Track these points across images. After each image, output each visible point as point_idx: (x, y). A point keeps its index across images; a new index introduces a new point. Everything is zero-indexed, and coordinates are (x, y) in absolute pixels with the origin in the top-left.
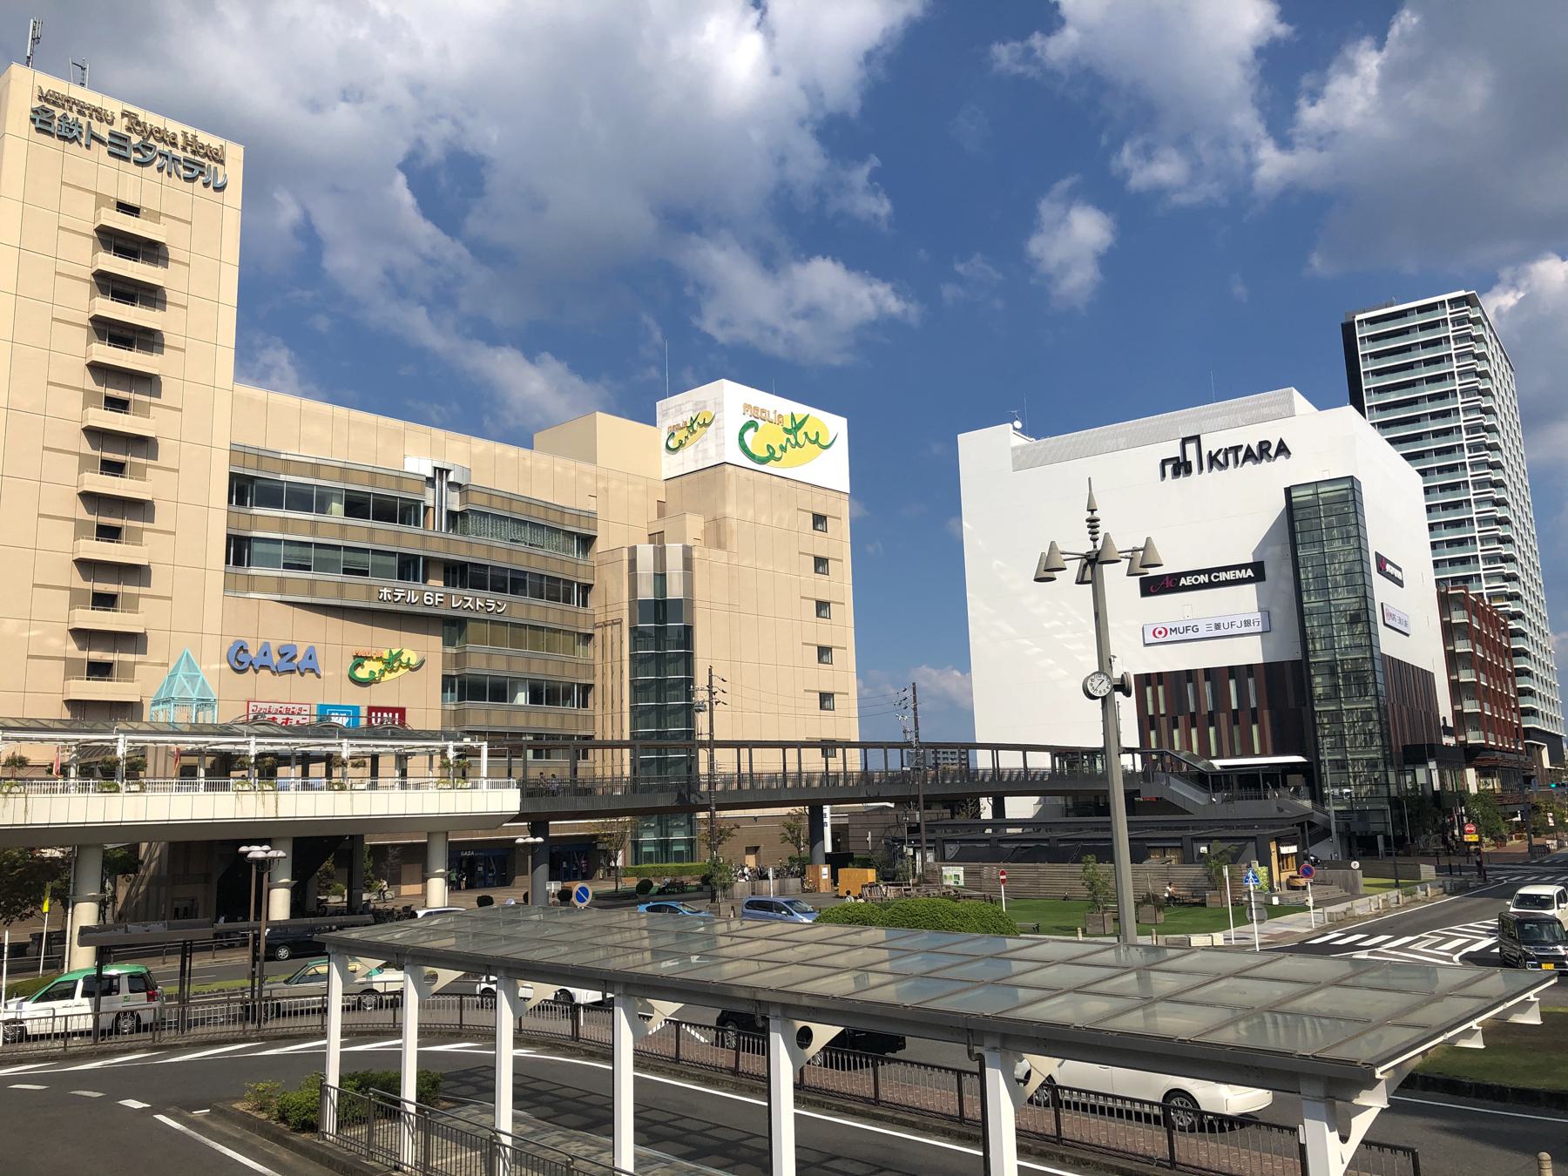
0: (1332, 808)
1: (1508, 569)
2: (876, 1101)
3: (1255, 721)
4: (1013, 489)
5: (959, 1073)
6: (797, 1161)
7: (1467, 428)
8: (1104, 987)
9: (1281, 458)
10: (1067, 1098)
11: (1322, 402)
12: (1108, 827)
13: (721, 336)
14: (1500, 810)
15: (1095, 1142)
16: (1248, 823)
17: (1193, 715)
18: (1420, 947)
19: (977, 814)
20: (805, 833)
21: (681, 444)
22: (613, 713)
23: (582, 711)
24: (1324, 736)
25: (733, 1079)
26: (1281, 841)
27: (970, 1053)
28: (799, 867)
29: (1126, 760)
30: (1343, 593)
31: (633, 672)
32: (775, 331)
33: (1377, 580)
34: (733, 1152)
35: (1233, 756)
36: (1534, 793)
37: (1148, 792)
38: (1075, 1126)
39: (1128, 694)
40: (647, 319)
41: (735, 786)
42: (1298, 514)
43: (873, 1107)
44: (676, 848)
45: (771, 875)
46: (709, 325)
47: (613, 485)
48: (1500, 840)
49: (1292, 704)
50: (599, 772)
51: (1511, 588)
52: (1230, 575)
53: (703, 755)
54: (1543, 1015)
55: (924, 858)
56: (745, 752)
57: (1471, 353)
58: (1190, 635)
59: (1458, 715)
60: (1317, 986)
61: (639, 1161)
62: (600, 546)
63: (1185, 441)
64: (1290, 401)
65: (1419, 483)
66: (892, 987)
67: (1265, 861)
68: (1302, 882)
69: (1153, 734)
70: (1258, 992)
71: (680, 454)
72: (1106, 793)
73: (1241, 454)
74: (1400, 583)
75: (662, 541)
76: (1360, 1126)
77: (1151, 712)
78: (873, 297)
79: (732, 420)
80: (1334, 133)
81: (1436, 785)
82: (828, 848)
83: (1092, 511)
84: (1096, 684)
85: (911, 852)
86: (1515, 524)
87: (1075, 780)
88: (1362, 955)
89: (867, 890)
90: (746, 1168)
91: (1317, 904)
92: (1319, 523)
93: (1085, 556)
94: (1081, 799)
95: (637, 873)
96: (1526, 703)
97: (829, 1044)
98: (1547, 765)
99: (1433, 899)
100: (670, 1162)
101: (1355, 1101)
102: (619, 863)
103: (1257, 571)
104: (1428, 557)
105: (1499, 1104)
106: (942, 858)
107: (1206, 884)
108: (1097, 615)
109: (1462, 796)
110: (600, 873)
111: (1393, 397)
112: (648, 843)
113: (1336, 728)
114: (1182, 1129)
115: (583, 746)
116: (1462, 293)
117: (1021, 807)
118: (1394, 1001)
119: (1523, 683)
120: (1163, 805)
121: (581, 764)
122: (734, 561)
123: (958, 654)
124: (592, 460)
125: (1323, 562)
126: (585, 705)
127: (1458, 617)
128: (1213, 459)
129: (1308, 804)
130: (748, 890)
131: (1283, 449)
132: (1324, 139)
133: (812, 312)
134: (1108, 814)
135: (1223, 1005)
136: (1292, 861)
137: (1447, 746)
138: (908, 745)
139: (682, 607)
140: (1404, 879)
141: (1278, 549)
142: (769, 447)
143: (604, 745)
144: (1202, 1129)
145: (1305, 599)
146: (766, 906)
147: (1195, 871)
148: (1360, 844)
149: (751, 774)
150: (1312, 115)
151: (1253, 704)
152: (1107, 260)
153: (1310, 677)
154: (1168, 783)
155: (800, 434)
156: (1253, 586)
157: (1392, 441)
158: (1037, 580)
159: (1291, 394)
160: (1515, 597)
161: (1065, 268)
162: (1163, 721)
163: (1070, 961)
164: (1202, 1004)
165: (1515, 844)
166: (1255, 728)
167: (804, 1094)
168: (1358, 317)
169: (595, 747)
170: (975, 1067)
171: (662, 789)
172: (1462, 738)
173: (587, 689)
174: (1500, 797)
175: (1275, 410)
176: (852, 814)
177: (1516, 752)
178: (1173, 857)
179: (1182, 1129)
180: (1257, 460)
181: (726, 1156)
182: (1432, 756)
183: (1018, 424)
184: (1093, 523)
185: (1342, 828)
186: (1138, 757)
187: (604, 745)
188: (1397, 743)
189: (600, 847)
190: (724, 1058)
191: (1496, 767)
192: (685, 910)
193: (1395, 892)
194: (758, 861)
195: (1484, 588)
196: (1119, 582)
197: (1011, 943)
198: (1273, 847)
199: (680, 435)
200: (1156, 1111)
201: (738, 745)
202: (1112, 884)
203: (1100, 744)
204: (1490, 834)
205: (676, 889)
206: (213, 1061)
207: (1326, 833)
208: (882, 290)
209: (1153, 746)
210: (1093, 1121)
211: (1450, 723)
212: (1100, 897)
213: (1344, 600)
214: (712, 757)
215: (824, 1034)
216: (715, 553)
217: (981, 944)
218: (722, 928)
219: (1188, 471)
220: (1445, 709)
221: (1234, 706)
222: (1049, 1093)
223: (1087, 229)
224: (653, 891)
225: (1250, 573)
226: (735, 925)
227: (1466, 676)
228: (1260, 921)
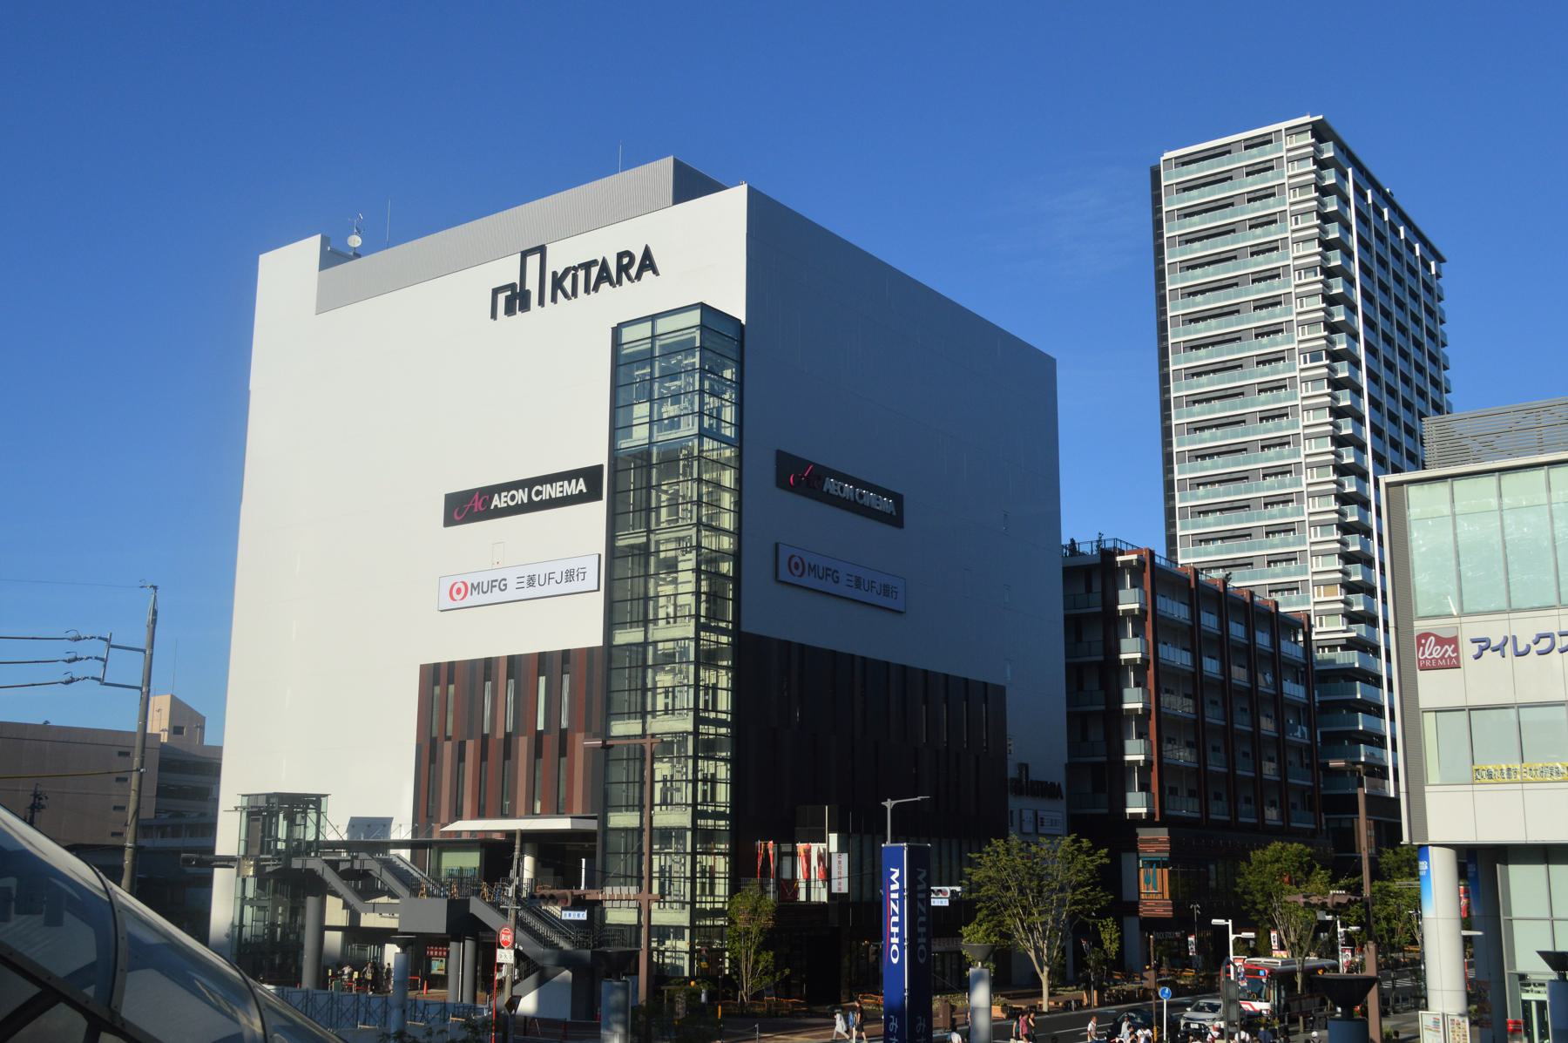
9: (648, 274)
73: (595, 271)
168: (1167, 155)
206: (1455, 463)
219: (525, 307)
221: (540, 727)
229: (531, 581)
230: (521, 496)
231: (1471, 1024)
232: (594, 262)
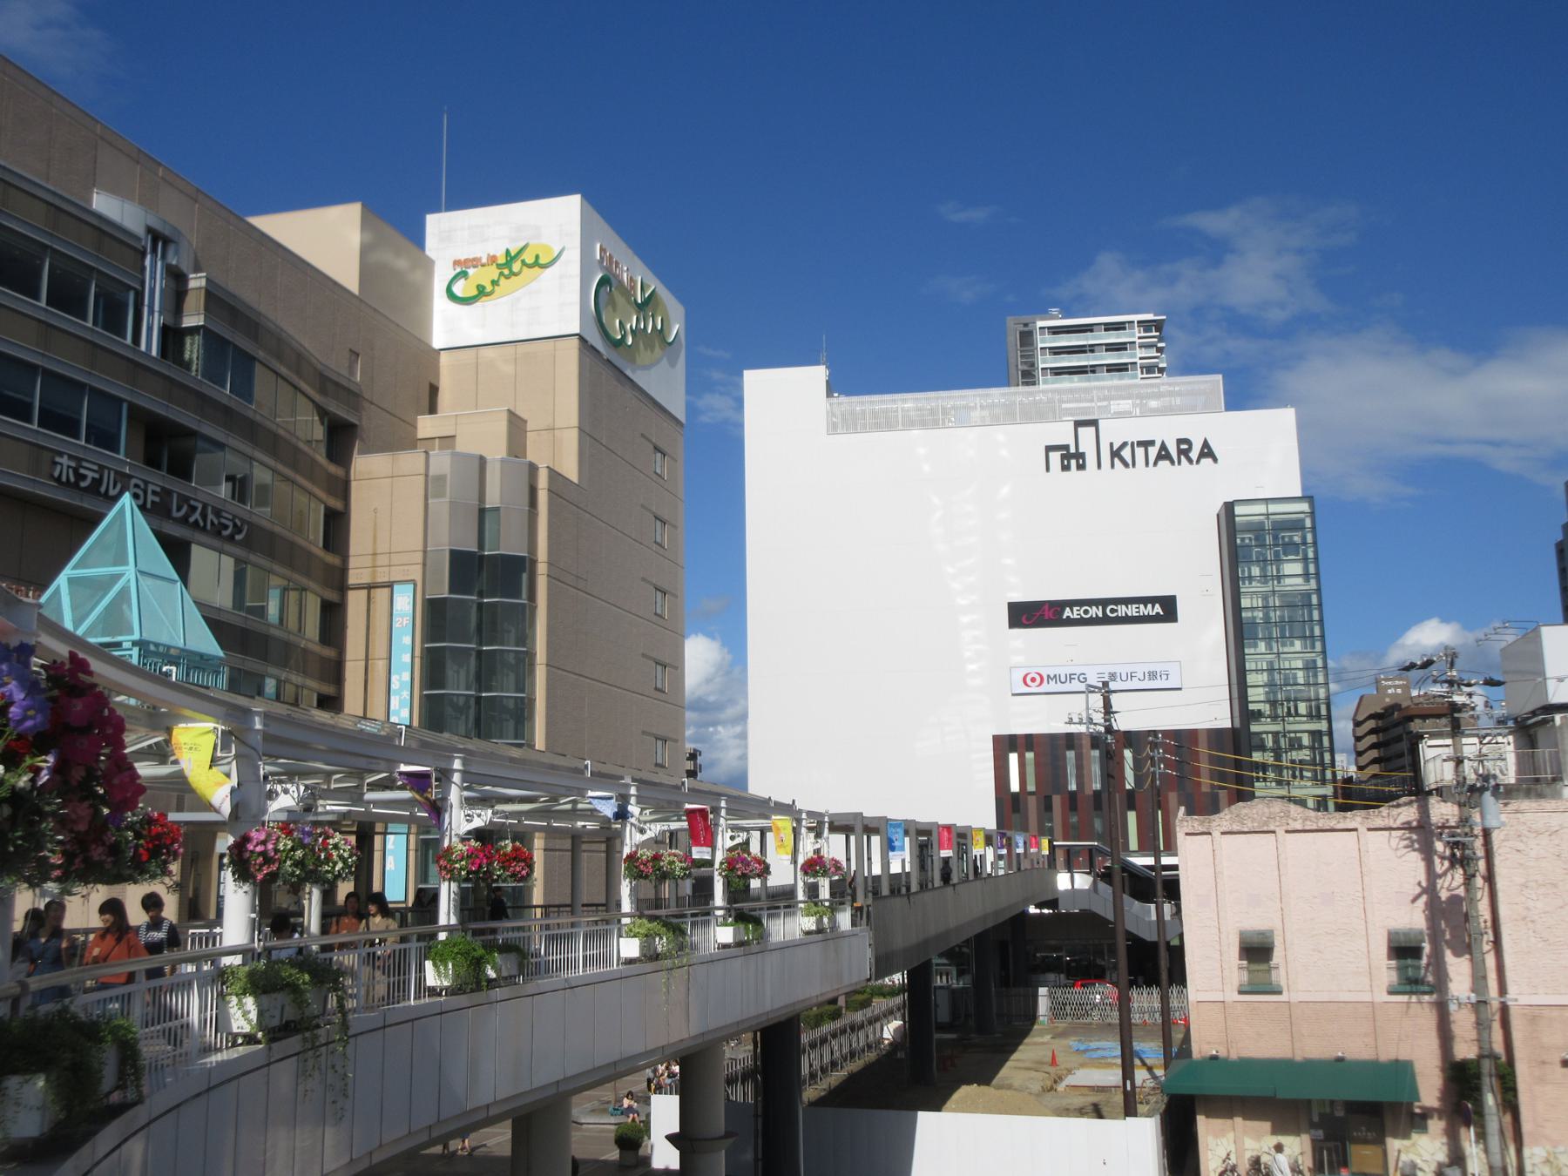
3: (1131, 807)
17: (1073, 795)
21: (482, 292)
52: (1132, 610)
73: (1153, 452)
116: (1150, 317)
128: (1116, 454)
131: (1207, 452)
168: (1040, 324)
199: (484, 276)
225: (1158, 609)
230: (1095, 611)
232: (1152, 443)
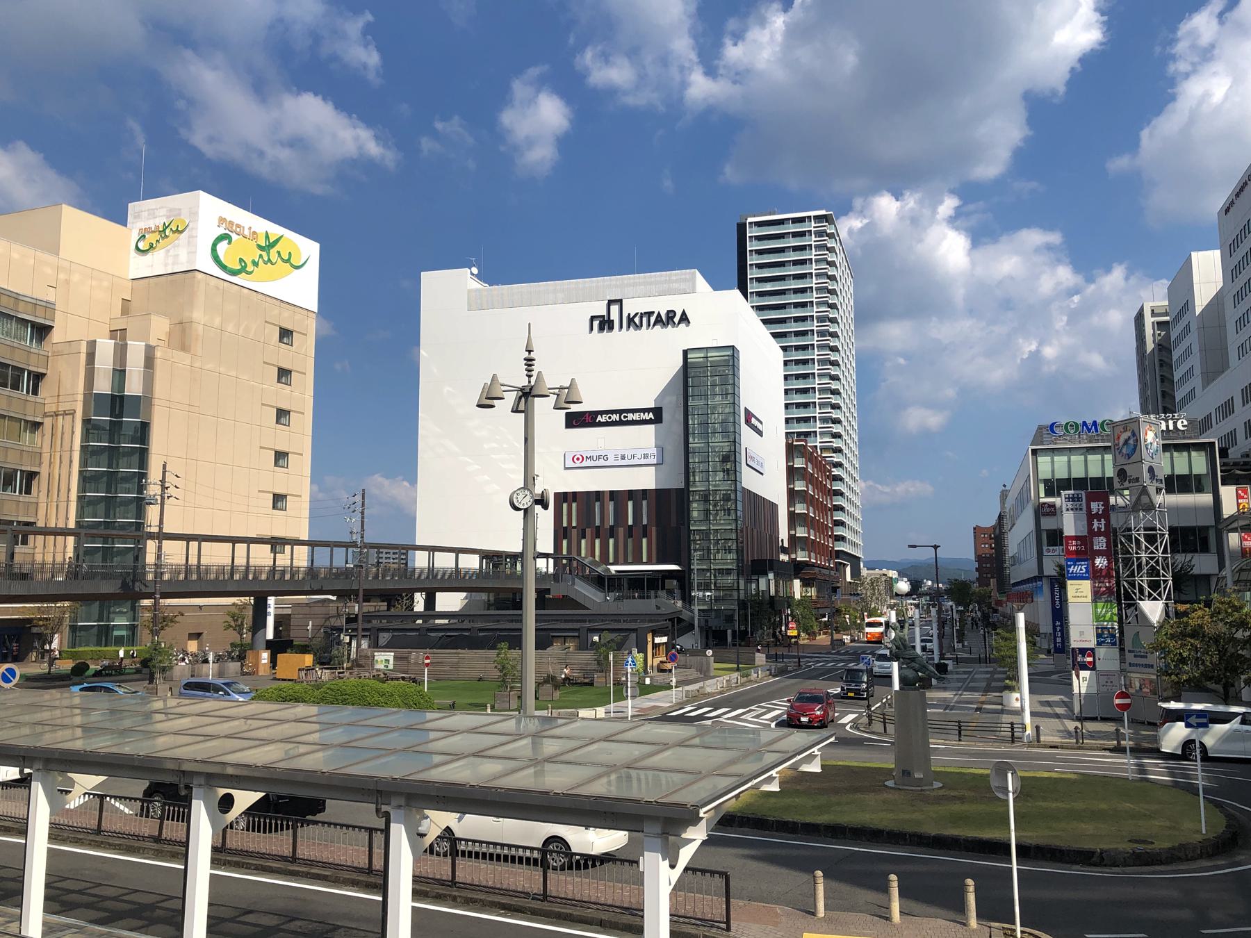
0: (696, 608)
1: (836, 429)
2: (294, 859)
3: (645, 536)
4: (465, 323)
5: (371, 831)
6: (210, 917)
7: (818, 318)
8: (499, 751)
9: (682, 325)
10: (463, 848)
11: (717, 284)
12: (520, 619)
13: (208, 150)
14: (814, 612)
15: (484, 883)
16: (634, 617)
18: (748, 717)
19: (410, 607)
20: (248, 622)
22: (59, 500)
23: (24, 498)
24: (695, 550)
25: (156, 846)
26: (656, 633)
27: (378, 811)
28: (241, 653)
29: (541, 563)
30: (718, 437)
31: (84, 463)
32: (261, 154)
33: (744, 429)
34: (148, 914)
35: (626, 563)
36: (839, 600)
37: (556, 591)
38: (468, 871)
39: (546, 507)
40: (134, 125)
41: (182, 577)
42: (691, 372)
43: (291, 865)
44: (116, 633)
45: (211, 659)
46: (198, 139)
47: (76, 278)
48: (812, 635)
49: (674, 524)
50: (39, 558)
51: (837, 443)
52: (636, 417)
53: (151, 546)
54: (823, 767)
55: (359, 646)
56: (194, 545)
57: (825, 260)
58: (602, 462)
59: (792, 538)
60: (665, 746)
61: (48, 929)
62: (56, 336)
63: (610, 303)
64: (693, 280)
65: (780, 356)
66: (320, 755)
67: (642, 649)
68: (669, 666)
69: (565, 542)
70: (620, 752)
71: (149, 256)
72: (521, 591)
73: (653, 319)
74: (760, 433)
75: (124, 338)
76: (686, 855)
77: (565, 524)
78: (357, 138)
79: (207, 230)
80: (748, 71)
81: (772, 592)
82: (270, 635)
83: (530, 352)
84: (520, 498)
85: (347, 639)
86: (844, 395)
87: (497, 580)
88: (709, 722)
89: (303, 673)
90: (160, 927)
91: (679, 684)
92: (705, 381)
93: (521, 390)
94: (502, 595)
95: (73, 656)
96: (839, 531)
97: (249, 809)
98: (848, 579)
99: (762, 680)
100: (81, 928)
101: (684, 836)
102: (55, 645)
103: (657, 415)
104: (782, 415)
105: (1059, 865)
106: (375, 645)
107: (595, 667)
108: (526, 440)
109: (789, 601)
110: (33, 656)
111: (768, 287)
112: (120, 627)
113: (705, 544)
114: (555, 869)
115: (25, 531)
117: (450, 602)
118: (719, 756)
119: (838, 516)
120: (567, 602)
121: (19, 549)
122: (198, 364)
123: (405, 464)
124: (54, 249)
125: (708, 410)
126: (28, 491)
127: (799, 463)
128: (631, 320)
129: (679, 604)
130: (188, 673)
131: (684, 318)
132: (740, 75)
133: (297, 143)
134: (521, 608)
135: (593, 764)
136: (663, 649)
137: (783, 562)
138: (354, 545)
139: (141, 404)
140: (743, 664)
141: (674, 398)
142: (241, 260)
143: (46, 532)
144: (570, 868)
145: (691, 440)
146: (204, 687)
147: (587, 657)
148: (715, 638)
149: (199, 566)
150: (733, 53)
151: (645, 522)
152: (564, 142)
153: (689, 502)
154: (574, 584)
155: (273, 251)
156: (653, 426)
157: (765, 322)
158: (479, 406)
159: (694, 274)
160: (838, 450)
161: (530, 142)
162: (574, 532)
163: (473, 730)
164: (576, 764)
165: (823, 639)
166: (644, 541)
167: (221, 854)
168: (750, 220)
169: (36, 533)
170: (381, 823)
171: (106, 577)
172: (793, 556)
173: (31, 476)
174: (815, 602)
175: (682, 286)
176: (296, 605)
177: (829, 568)
178: (571, 644)
179: (555, 869)
180: (665, 325)
181: (140, 918)
182: (771, 569)
183: (475, 270)
184: (529, 362)
185: (703, 624)
186: (551, 561)
187: (46, 532)
188: (748, 558)
189: (35, 630)
190: (148, 827)
191: (814, 579)
192: (121, 691)
193: (736, 674)
194: (200, 646)
195: (818, 442)
196: (547, 414)
197: (430, 715)
198: (650, 639)
199: (151, 238)
200: (536, 854)
201: (188, 538)
202: (519, 668)
203: (517, 548)
204: (806, 630)
205: (114, 672)
207: (691, 627)
208: (365, 134)
209: (565, 552)
210: (483, 866)
211: (786, 545)
212: (508, 678)
213: (719, 443)
214: (160, 548)
215: (245, 799)
216: (179, 355)
217: (398, 717)
218: (158, 705)
219: (611, 328)
220: (784, 534)
221: (630, 522)
222: (448, 845)
223: (550, 113)
224: (90, 672)
226: (172, 702)
227: (800, 509)
228: (633, 697)
229: (623, 457)
230: (615, 417)
231: (1097, 595)
